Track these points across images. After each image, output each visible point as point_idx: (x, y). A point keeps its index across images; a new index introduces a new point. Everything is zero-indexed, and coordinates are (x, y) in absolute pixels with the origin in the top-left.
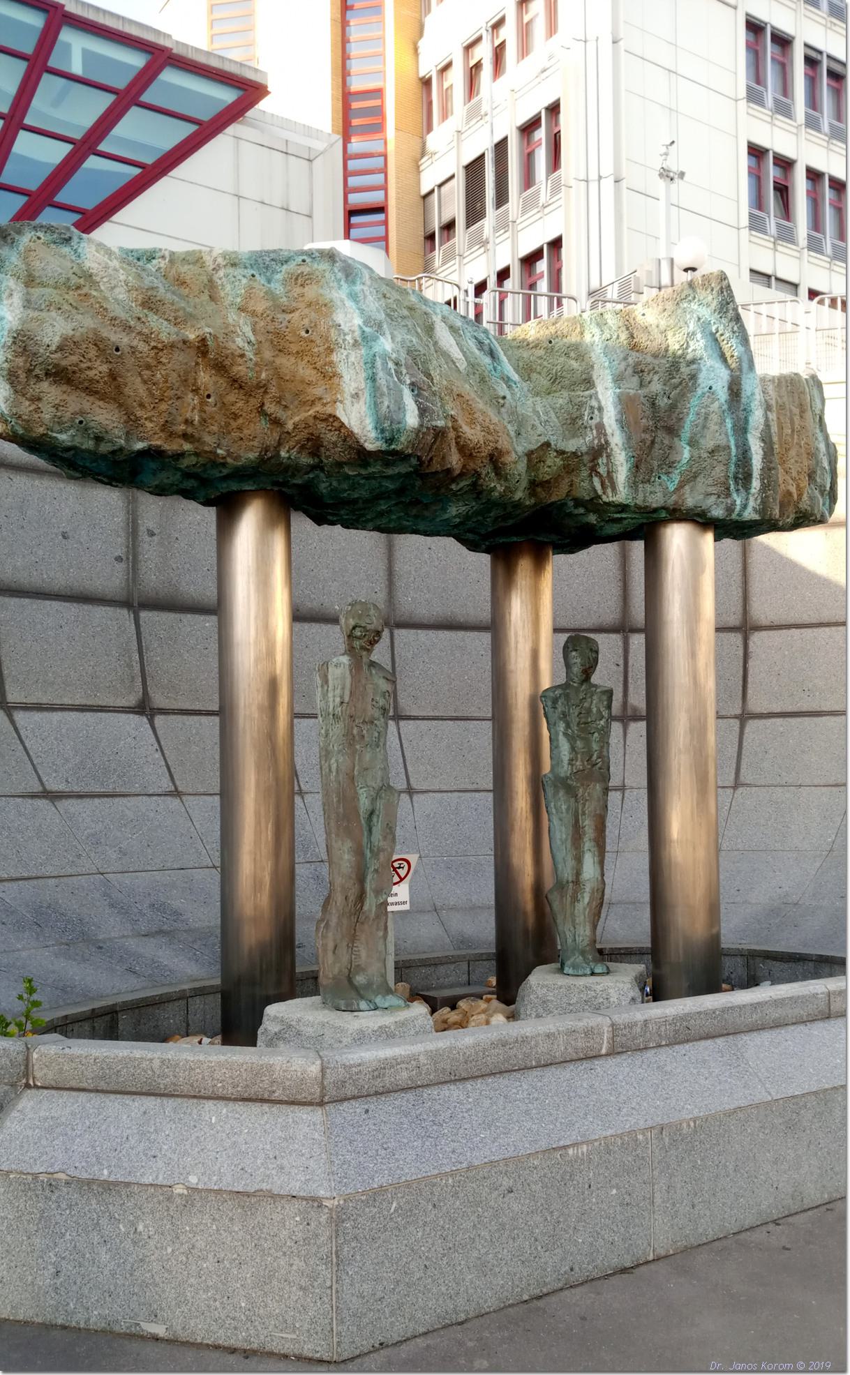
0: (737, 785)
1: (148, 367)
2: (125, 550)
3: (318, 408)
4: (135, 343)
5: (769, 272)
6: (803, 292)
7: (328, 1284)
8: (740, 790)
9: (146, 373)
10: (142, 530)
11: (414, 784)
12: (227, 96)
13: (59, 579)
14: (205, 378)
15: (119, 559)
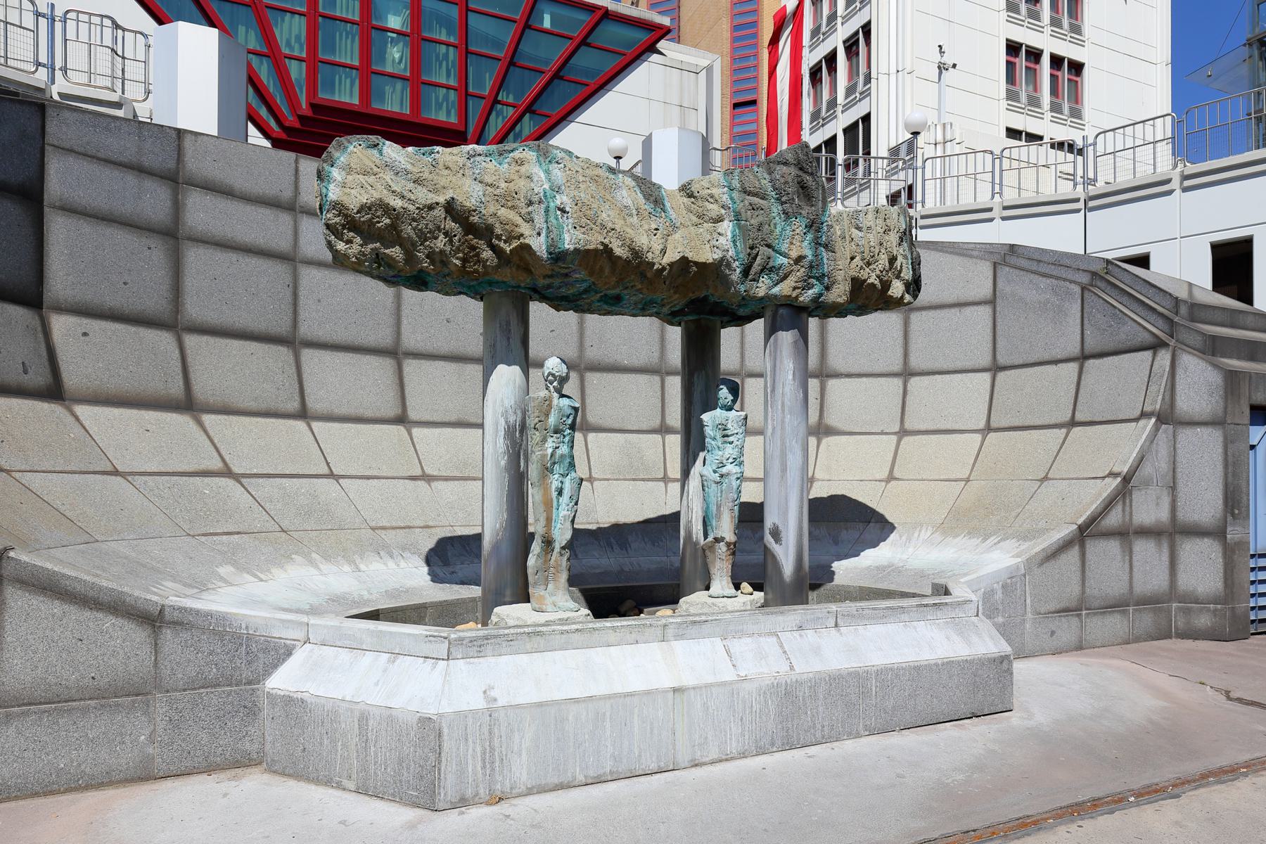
0: (891, 478)
1: (414, 220)
5: (1021, 128)
8: (893, 483)
9: (415, 224)
11: (594, 475)
12: (642, 36)
14: (450, 225)
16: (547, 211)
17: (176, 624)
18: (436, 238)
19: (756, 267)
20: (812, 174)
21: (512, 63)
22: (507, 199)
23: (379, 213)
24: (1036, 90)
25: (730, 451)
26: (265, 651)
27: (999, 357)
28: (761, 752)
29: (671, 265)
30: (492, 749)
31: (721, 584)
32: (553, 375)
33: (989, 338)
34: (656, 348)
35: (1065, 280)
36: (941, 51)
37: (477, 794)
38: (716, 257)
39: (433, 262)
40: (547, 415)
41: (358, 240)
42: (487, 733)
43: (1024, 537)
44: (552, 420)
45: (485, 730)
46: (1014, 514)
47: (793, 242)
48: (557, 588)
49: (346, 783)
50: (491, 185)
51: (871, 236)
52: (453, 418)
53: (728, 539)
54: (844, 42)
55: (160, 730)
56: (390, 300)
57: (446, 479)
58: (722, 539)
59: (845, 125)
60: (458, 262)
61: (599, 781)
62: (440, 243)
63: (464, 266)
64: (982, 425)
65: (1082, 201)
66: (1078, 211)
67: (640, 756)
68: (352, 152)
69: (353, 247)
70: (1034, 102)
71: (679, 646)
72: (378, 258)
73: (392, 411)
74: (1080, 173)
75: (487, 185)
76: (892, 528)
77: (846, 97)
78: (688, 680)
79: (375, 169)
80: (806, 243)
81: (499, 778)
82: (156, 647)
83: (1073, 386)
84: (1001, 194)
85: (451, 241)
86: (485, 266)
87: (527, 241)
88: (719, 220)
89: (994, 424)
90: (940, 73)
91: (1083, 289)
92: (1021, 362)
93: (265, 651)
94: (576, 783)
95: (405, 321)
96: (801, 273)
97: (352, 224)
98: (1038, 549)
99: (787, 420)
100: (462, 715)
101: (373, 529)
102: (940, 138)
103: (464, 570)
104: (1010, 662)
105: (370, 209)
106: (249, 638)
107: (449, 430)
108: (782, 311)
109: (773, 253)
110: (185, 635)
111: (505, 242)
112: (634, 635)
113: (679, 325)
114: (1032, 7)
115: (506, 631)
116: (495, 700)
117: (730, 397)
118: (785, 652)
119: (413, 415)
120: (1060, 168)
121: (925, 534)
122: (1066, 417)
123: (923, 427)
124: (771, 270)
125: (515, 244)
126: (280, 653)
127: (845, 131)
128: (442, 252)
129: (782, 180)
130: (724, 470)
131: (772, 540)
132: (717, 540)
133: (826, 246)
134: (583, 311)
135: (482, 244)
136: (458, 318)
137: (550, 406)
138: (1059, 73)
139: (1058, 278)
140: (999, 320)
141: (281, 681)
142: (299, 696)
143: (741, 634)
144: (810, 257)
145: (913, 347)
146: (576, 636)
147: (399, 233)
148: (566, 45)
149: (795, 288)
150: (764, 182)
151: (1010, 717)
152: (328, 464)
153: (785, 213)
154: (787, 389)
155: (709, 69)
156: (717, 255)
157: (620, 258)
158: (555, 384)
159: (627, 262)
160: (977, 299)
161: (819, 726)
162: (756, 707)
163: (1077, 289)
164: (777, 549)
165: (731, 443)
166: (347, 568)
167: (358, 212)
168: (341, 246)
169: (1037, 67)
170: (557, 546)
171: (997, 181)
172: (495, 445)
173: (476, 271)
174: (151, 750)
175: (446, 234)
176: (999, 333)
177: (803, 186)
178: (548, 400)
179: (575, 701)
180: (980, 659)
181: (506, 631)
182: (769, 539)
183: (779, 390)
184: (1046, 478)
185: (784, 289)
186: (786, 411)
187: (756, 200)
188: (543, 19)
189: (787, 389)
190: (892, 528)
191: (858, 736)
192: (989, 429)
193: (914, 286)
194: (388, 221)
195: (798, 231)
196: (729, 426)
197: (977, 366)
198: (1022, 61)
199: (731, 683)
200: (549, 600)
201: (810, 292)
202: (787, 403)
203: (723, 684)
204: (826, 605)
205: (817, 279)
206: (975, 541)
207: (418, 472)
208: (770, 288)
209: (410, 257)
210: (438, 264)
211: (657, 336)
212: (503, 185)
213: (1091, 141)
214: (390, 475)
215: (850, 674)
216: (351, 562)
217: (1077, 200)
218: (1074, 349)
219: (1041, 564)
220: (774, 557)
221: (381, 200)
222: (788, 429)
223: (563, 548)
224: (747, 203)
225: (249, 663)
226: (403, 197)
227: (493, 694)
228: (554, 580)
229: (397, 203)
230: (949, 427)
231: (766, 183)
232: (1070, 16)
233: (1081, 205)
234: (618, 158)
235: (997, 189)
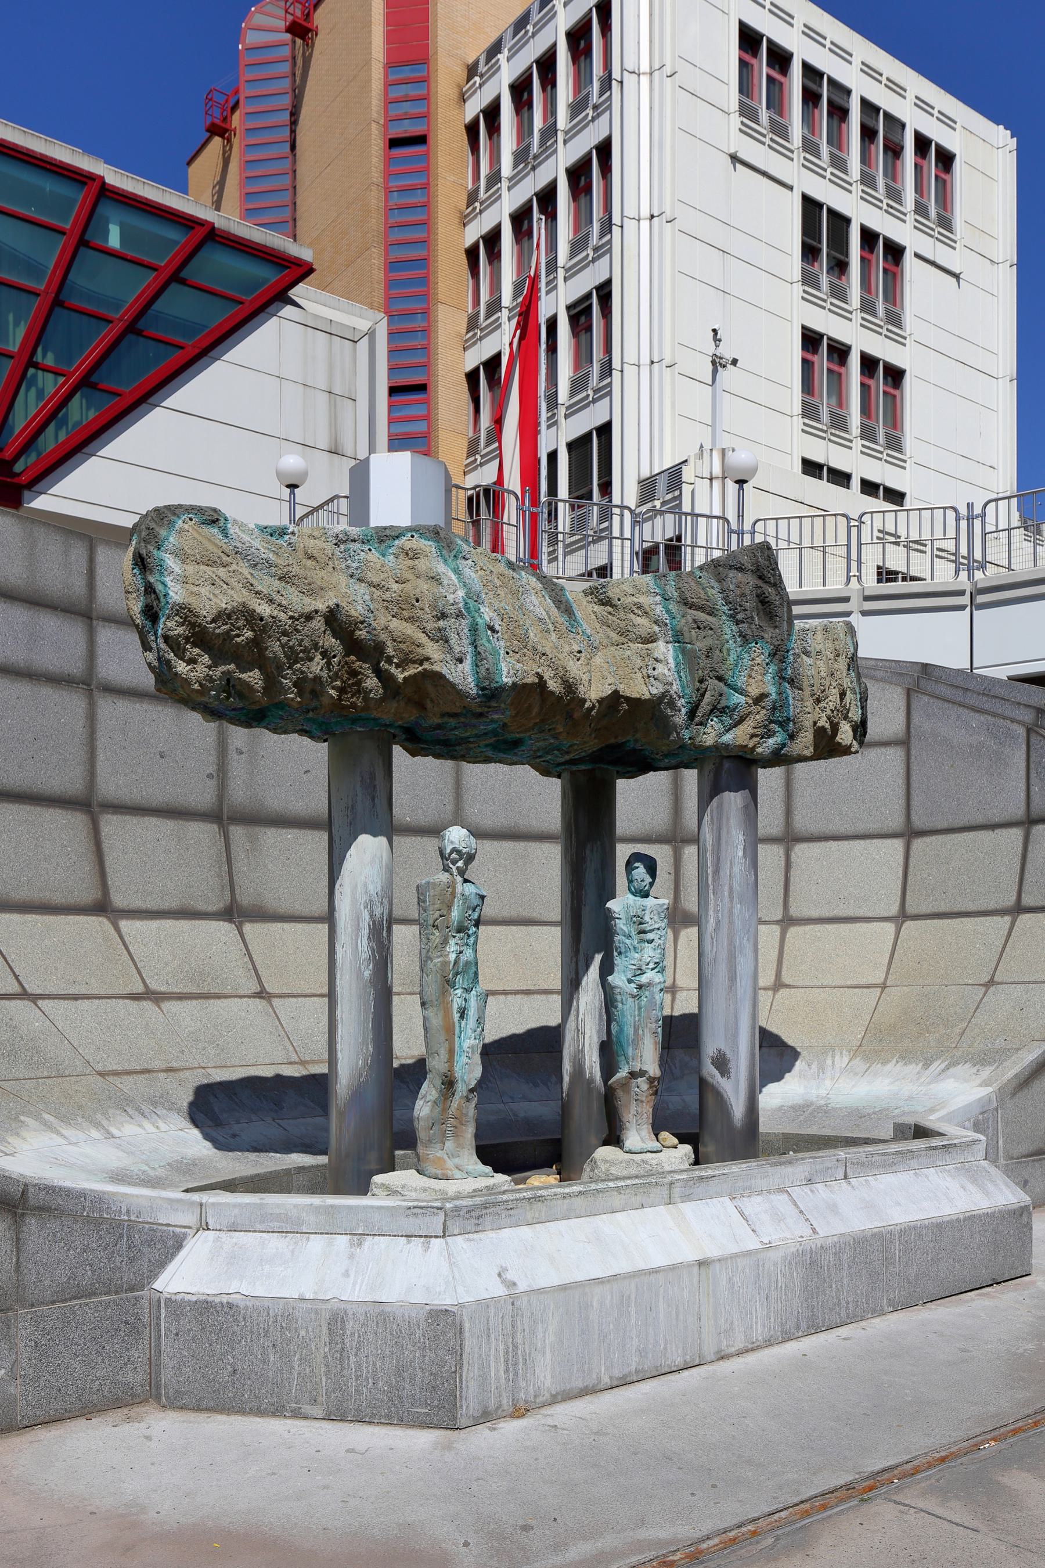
1: (285, 633)
2: (215, 767)
3: (426, 666)
4: (275, 613)
6: (856, 483)
7: (453, 1369)
8: (783, 992)
10: (232, 748)
13: (157, 796)
14: (330, 642)
15: (210, 776)
16: (474, 629)
17: (43, 1210)
18: (311, 659)
19: (704, 707)
20: (775, 585)
21: (58, 302)
22: (405, 607)
23: (240, 623)
24: (840, 405)
25: (649, 953)
26: (150, 1243)
27: (914, 818)
28: (787, 1338)
29: (601, 701)
30: (515, 1346)
31: (637, 1135)
32: (459, 852)
33: (901, 791)
34: (449, 799)
35: (1004, 718)
36: (717, 339)
37: (500, 1406)
38: (654, 691)
39: (300, 693)
40: (450, 907)
41: (206, 659)
42: (509, 1327)
43: (981, 1060)
44: (455, 914)
45: (508, 1322)
46: (957, 1030)
47: (753, 676)
48: (460, 1146)
49: (307, 1409)
50: (377, 586)
51: (820, 663)
52: (173, 904)
53: (651, 1073)
54: (569, 308)
55: (23, 1361)
56: (81, 723)
57: (181, 997)
58: (642, 1073)
59: (570, 438)
60: (332, 692)
61: (624, 1382)
62: (316, 666)
63: (340, 699)
64: (894, 910)
65: (968, 594)
66: (962, 608)
67: (665, 1349)
68: (181, 531)
69: (195, 669)
70: (839, 422)
71: (687, 1208)
72: (229, 684)
73: (88, 895)
74: (963, 551)
75: (371, 585)
76: (795, 1055)
77: (572, 395)
78: (712, 1252)
79: (225, 558)
80: (769, 677)
81: (522, 1384)
82: (18, 1244)
83: (1017, 860)
84: (859, 578)
85: (329, 664)
86: (366, 699)
87: (436, 668)
88: (651, 639)
89: (910, 910)
90: (715, 372)
91: (1029, 731)
92: (945, 825)
93: (150, 1243)
94: (601, 1386)
95: (101, 757)
96: (762, 715)
97: (200, 636)
98: (1010, 1074)
99: (736, 911)
100: (483, 1304)
101: (102, 1074)
102: (717, 470)
103: (297, 1127)
104: (1030, 1214)
105: (229, 616)
106: (132, 1225)
107: (169, 924)
108: (727, 765)
109: (725, 689)
110: (54, 1225)
111: (397, 666)
112: (639, 1197)
113: (559, 777)
114: (836, 281)
115: (505, 1197)
116: (514, 1284)
117: (649, 879)
118: (801, 1212)
119: (118, 900)
120: (937, 545)
121: (842, 1060)
122: (1010, 900)
123: (815, 913)
124: (723, 710)
125: (412, 670)
126: (168, 1245)
127: (570, 446)
128: (317, 679)
129: (738, 592)
130: (644, 979)
131: (716, 1073)
132: (633, 1075)
133: (791, 682)
134: (463, 758)
135: (366, 668)
136: (294, 766)
137: (453, 894)
138: (871, 382)
139: (994, 715)
140: (914, 767)
141: (183, 1277)
142: (225, 1299)
143: (751, 1192)
144: (774, 696)
145: (798, 802)
146: (578, 1201)
147: (262, 650)
148: (146, 279)
149: (752, 736)
150: (711, 592)
151: (1033, 1283)
152: (17, 977)
153: (743, 636)
154: (736, 869)
155: (371, 334)
156: (656, 689)
157: (553, 693)
158: (460, 864)
159: (560, 698)
160: (885, 738)
161: (844, 1303)
162: (781, 1281)
163: (1021, 731)
164: (725, 1085)
165: (651, 942)
166: (95, 1134)
167: (213, 621)
168: (181, 667)
169: (843, 370)
170: (461, 1089)
171: (854, 556)
172: (354, 948)
173: (353, 705)
174: (12, 1390)
175: (324, 654)
176: (914, 784)
177: (763, 601)
178: (452, 886)
179: (599, 1281)
180: (1000, 1212)
181: (505, 1197)
182: (710, 1071)
183: (725, 870)
184: (991, 983)
185: (739, 736)
186: (736, 899)
187: (701, 616)
188: (106, 233)
189: (736, 869)
190: (795, 1055)
191: (882, 1314)
192: (903, 916)
193: (860, 729)
194: (249, 634)
195: (758, 660)
196: (647, 918)
197: (885, 830)
198: (822, 360)
199: (757, 1251)
200: (450, 1163)
201: (771, 741)
202: (736, 888)
203: (748, 1253)
204: (832, 1152)
205: (780, 724)
206: (913, 1069)
207: (140, 988)
208: (720, 735)
209: (271, 683)
210: (307, 695)
211: (450, 780)
212: (395, 587)
213: (977, 510)
214: (102, 992)
215: (873, 1235)
216: (98, 1125)
217: (961, 593)
218: (1017, 810)
219: (1014, 1094)
220: (718, 1095)
221: (244, 605)
222: (738, 923)
223: (472, 1091)
224: (690, 618)
225: (132, 1260)
226: (271, 601)
227: (509, 1276)
228: (456, 1135)
229: (264, 609)
230: (850, 913)
231: (714, 593)
232: (886, 299)
233: (965, 600)
234: (292, 487)
235: (854, 571)
